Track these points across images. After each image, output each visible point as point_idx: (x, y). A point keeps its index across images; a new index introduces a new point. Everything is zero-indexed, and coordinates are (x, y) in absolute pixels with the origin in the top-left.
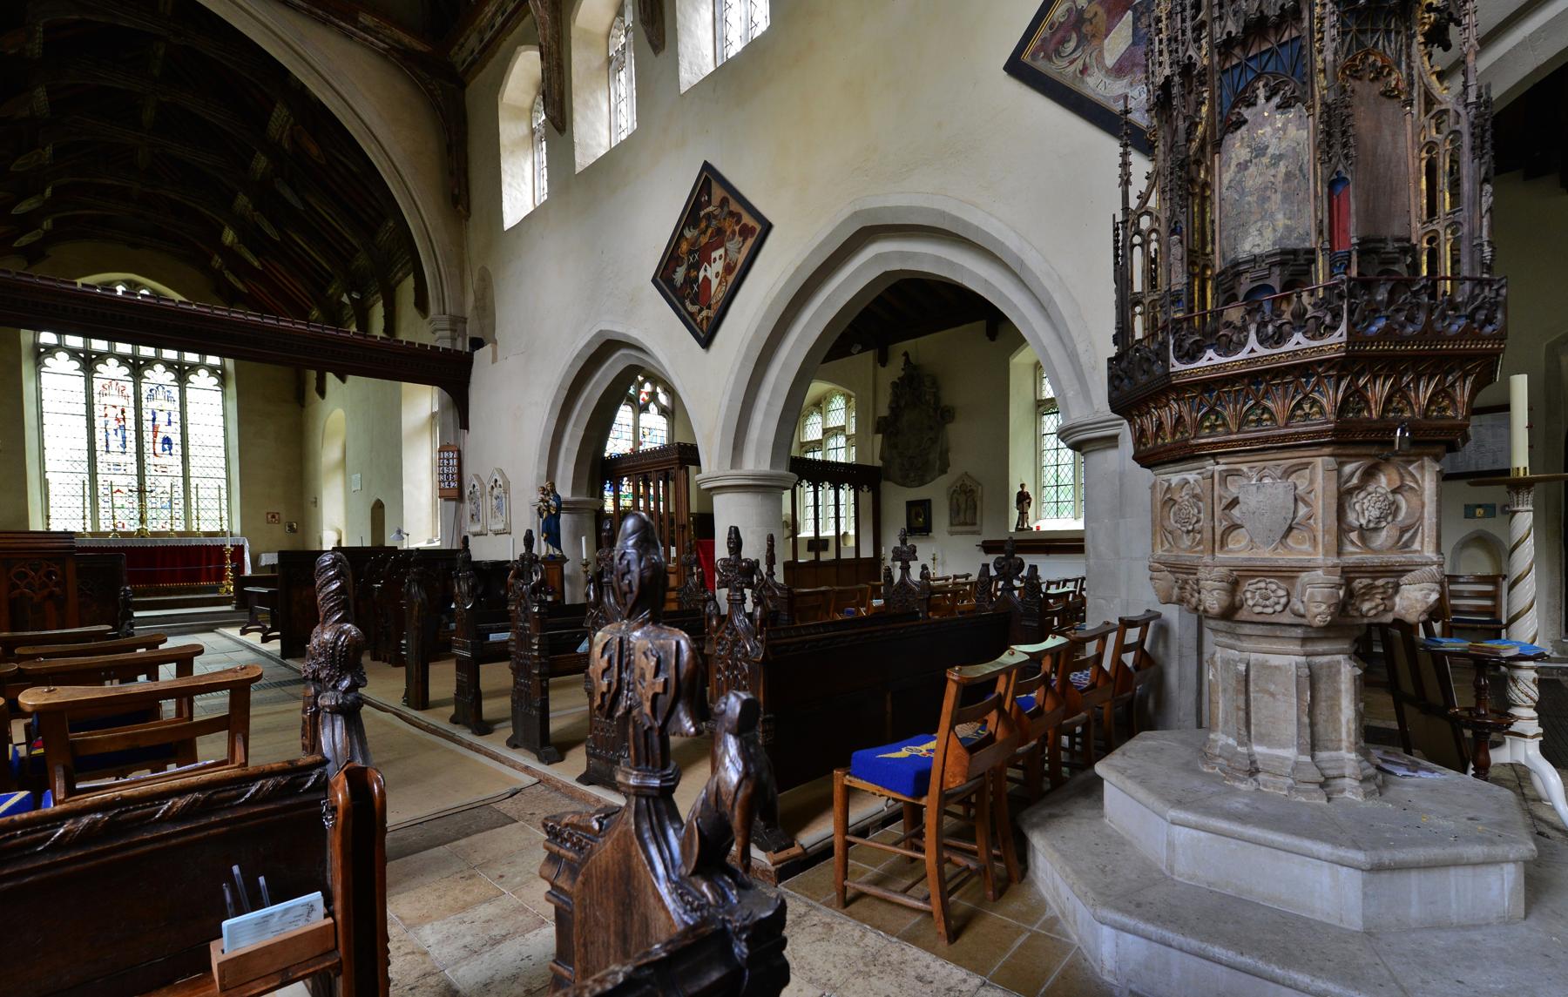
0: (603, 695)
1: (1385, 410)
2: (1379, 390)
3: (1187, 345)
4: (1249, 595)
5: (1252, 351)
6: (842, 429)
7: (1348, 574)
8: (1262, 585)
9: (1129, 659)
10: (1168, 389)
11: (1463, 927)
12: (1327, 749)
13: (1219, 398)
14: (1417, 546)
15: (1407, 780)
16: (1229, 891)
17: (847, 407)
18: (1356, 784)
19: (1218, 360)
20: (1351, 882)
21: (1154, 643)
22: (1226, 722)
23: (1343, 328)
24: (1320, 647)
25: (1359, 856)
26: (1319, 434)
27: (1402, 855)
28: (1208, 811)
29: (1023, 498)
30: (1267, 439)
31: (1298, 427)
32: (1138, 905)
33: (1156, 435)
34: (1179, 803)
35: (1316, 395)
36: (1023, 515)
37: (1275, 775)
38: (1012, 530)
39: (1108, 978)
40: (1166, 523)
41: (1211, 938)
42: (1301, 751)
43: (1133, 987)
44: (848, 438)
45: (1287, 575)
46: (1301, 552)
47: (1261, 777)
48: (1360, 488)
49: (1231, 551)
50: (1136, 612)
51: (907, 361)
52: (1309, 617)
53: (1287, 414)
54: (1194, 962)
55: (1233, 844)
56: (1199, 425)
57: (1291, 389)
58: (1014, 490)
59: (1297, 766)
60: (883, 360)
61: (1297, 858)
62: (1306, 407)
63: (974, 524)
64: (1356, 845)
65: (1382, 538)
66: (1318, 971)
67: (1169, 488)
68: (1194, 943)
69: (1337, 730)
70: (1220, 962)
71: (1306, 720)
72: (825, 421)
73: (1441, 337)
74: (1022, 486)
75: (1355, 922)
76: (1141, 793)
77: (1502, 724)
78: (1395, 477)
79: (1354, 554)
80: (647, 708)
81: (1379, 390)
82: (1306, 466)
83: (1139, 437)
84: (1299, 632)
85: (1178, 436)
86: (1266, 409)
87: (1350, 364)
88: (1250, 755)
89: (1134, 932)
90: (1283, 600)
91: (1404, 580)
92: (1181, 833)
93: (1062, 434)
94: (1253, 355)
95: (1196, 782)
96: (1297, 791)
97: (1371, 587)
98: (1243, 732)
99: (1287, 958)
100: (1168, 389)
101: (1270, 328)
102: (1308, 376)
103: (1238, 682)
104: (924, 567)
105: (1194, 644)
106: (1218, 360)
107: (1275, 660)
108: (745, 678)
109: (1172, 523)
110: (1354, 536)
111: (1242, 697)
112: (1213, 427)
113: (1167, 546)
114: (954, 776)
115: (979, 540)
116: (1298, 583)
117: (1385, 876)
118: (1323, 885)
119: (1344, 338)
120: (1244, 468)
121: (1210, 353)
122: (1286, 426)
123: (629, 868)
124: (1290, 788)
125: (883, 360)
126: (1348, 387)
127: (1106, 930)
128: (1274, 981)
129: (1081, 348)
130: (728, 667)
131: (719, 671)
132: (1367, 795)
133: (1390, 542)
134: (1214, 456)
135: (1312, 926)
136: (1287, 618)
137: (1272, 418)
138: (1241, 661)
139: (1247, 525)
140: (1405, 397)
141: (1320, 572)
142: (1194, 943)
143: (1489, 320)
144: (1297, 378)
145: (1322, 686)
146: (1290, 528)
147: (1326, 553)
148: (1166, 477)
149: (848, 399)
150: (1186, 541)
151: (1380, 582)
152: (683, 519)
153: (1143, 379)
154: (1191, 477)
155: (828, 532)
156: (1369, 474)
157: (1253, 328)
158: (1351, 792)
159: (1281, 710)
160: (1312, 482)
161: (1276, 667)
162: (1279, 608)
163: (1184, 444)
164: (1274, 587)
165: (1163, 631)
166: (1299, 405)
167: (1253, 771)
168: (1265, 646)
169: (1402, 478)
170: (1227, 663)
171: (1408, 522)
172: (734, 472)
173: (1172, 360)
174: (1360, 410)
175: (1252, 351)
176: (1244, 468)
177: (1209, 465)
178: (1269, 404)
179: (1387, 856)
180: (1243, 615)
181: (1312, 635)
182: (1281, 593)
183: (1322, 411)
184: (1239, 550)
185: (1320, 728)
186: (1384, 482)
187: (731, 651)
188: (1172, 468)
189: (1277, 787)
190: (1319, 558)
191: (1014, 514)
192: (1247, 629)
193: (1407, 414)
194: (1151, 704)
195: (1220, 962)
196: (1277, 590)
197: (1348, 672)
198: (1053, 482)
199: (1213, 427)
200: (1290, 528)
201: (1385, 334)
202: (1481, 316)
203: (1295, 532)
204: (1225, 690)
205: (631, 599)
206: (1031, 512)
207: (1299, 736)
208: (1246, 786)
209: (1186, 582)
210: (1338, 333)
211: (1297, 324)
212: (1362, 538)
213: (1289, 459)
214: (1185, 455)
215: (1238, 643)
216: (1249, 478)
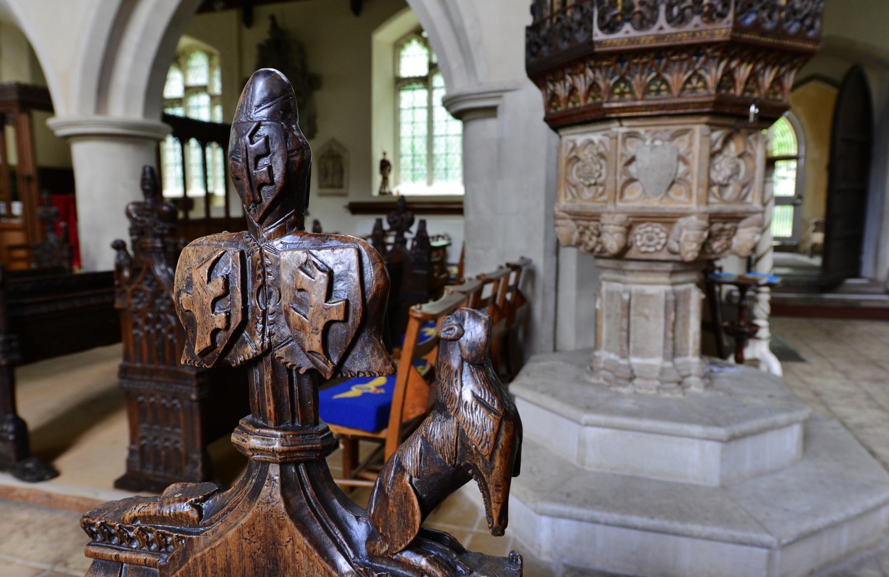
0: (216, 331)
1: (745, 90)
2: (743, 72)
3: (608, 18)
4: (638, 237)
5: (661, 28)
6: (203, 89)
7: (714, 218)
8: (649, 229)
9: (509, 296)
10: (589, 56)
11: (773, 472)
12: (680, 355)
13: (629, 68)
14: (749, 199)
15: (721, 374)
16: (627, 473)
17: (211, 67)
18: (697, 380)
19: (634, 33)
20: (713, 449)
21: (524, 284)
22: (608, 342)
23: (730, 16)
24: (681, 278)
25: (722, 432)
26: (703, 104)
27: (746, 426)
28: (612, 412)
29: (385, 166)
30: (657, 107)
31: (688, 98)
32: (568, 495)
33: (568, 99)
34: (588, 409)
35: (702, 72)
36: (385, 180)
37: (647, 379)
38: (376, 192)
39: (545, 558)
40: (570, 178)
41: (629, 509)
42: (665, 357)
43: (565, 561)
44: (213, 97)
45: (668, 220)
46: (680, 202)
47: (637, 382)
48: (720, 152)
49: (628, 201)
50: (515, 260)
51: (274, 26)
52: (683, 253)
53: (680, 86)
54: (614, 532)
55: (630, 435)
56: (611, 91)
57: (685, 66)
58: (377, 158)
59: (663, 371)
60: (248, 20)
61: (677, 440)
62: (694, 81)
63: (341, 186)
64: (716, 424)
65: (729, 193)
66: (705, 520)
67: (574, 148)
68: (616, 517)
69: (686, 341)
70: (636, 528)
71: (670, 335)
72: (185, 76)
73: (785, 35)
74: (385, 154)
75: (714, 480)
76: (556, 405)
77: (753, 332)
78: (741, 144)
79: (716, 206)
80: (314, 342)
81: (743, 72)
82: (685, 132)
83: (551, 100)
84: (669, 267)
85: (590, 101)
86: (664, 81)
87: (731, 49)
88: (630, 366)
89: (570, 517)
90: (663, 241)
91: (743, 223)
92: (592, 433)
93: (447, 103)
94: (662, 32)
95: (591, 392)
96: (665, 389)
97: (722, 230)
98: (625, 348)
99: (683, 516)
100: (589, 56)
101: (675, 11)
102: (699, 55)
103: (623, 309)
104: (316, 223)
105: (553, 284)
106: (634, 33)
107: (650, 290)
108: (171, 331)
109: (574, 178)
110: (715, 189)
111: (625, 321)
112: (622, 94)
113: (570, 197)
114: (414, 407)
115: (346, 201)
116: (676, 228)
117: (733, 444)
118: (692, 457)
119: (731, 25)
120: (642, 131)
121: (627, 27)
122: (679, 96)
123: (275, 561)
124: (658, 388)
125: (248, 20)
126: (725, 68)
127: (545, 520)
128: (676, 534)
129: (468, 23)
130: (147, 321)
131: (136, 325)
132: (707, 387)
133: (735, 196)
134: (620, 119)
135: (687, 488)
136: (664, 256)
137: (669, 89)
138: (625, 291)
139: (642, 179)
140: (756, 81)
141: (694, 218)
142: (616, 517)
143: (811, 27)
144: (690, 56)
145: (680, 308)
146: (673, 183)
147: (699, 203)
148: (572, 137)
149: (210, 56)
150: (588, 194)
151: (728, 226)
152: (30, 170)
153: (565, 45)
154: (596, 137)
155: (196, 191)
156: (726, 142)
157: (662, 8)
158: (696, 386)
159: (652, 328)
160: (690, 145)
161: (651, 296)
162: (659, 247)
163: (597, 107)
164: (657, 230)
165: (532, 274)
166: (689, 81)
167: (631, 378)
168: (643, 278)
169: (745, 146)
170: (611, 294)
171: (746, 180)
172: (99, 118)
173: (596, 29)
174: (728, 89)
175: (661, 28)
176: (642, 131)
177: (618, 129)
178: (667, 76)
179: (737, 429)
180: (632, 254)
181: (682, 266)
182: (663, 235)
183: (705, 86)
184: (634, 200)
185: (678, 340)
186: (733, 148)
187: (152, 305)
188: (580, 129)
189: (647, 388)
190: (693, 206)
191: (377, 179)
192: (632, 266)
193: (756, 95)
194: (520, 335)
195: (636, 528)
196: (658, 230)
197: (696, 297)
198: (409, 152)
199: (622, 94)
200: (673, 183)
201: (757, 26)
202: (808, 22)
203: (675, 186)
204: (608, 316)
205: (267, 196)
206: (391, 177)
207: (665, 347)
208: (626, 390)
209: (587, 228)
210: (725, 20)
211: (696, 8)
212: (720, 192)
213: (676, 125)
214: (596, 116)
215: (622, 278)
216: (644, 140)
